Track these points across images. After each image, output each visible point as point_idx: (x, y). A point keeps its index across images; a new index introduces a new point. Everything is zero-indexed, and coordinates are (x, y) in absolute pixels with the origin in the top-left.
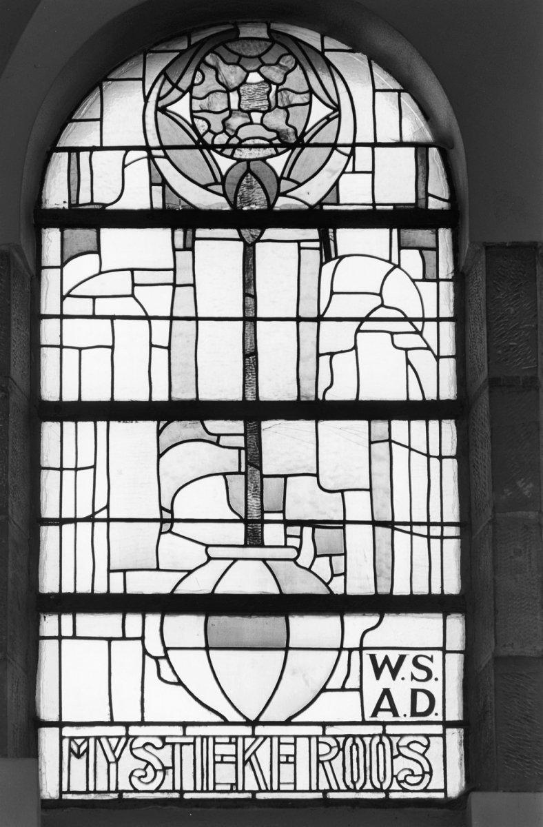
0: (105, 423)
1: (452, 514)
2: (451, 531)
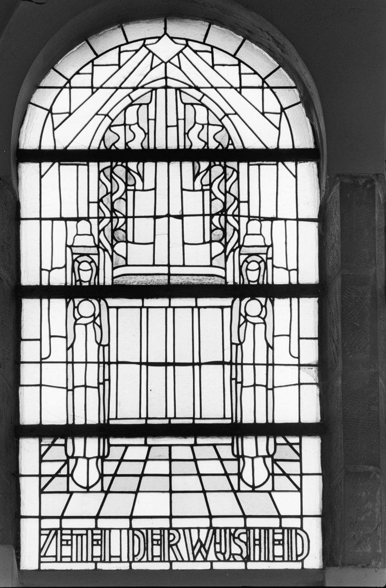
1: (174, 280)
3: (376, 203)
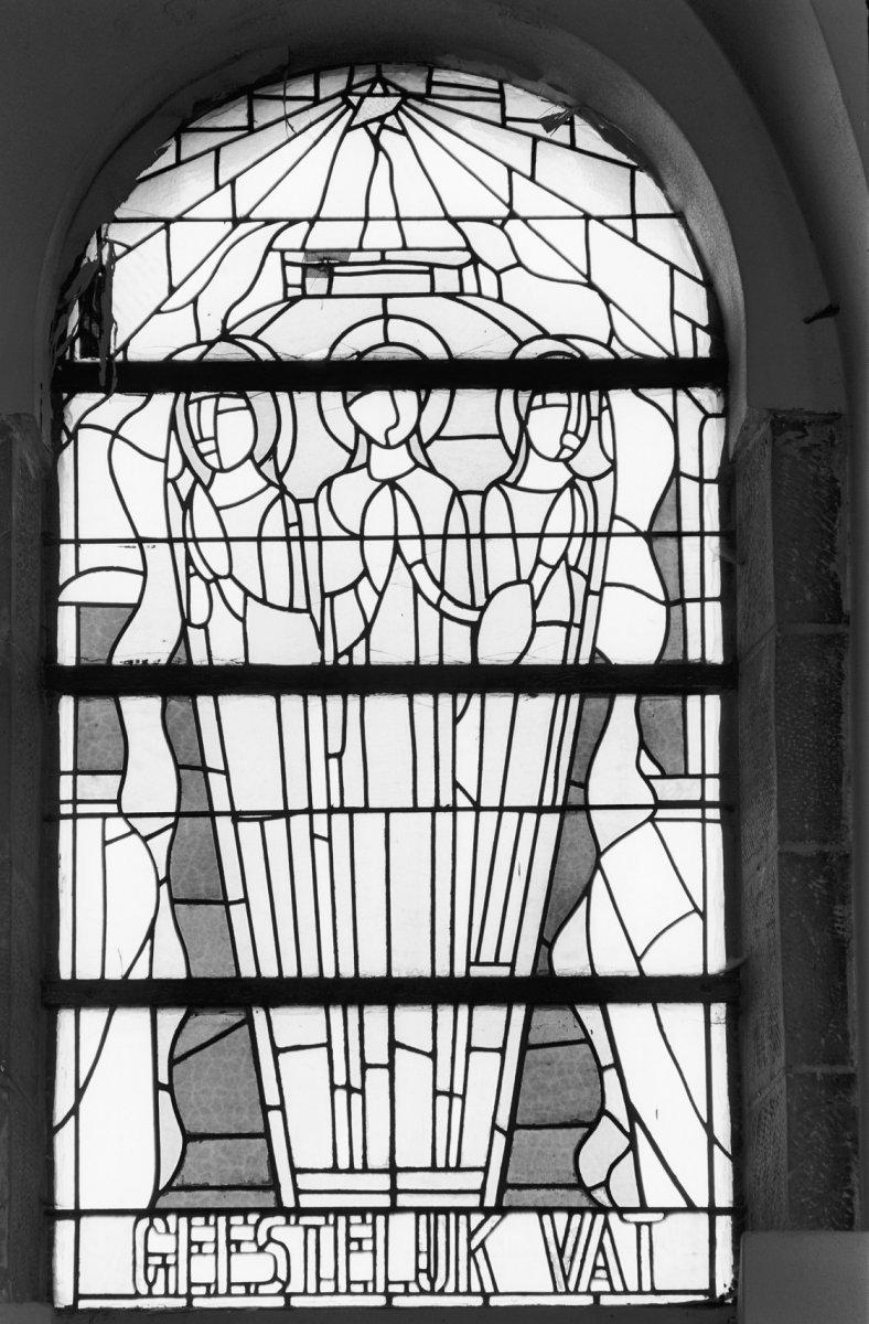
0: (285, 974)
2: (713, 813)
3: (14, 481)
